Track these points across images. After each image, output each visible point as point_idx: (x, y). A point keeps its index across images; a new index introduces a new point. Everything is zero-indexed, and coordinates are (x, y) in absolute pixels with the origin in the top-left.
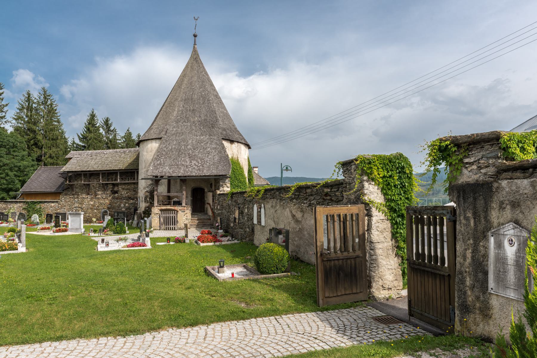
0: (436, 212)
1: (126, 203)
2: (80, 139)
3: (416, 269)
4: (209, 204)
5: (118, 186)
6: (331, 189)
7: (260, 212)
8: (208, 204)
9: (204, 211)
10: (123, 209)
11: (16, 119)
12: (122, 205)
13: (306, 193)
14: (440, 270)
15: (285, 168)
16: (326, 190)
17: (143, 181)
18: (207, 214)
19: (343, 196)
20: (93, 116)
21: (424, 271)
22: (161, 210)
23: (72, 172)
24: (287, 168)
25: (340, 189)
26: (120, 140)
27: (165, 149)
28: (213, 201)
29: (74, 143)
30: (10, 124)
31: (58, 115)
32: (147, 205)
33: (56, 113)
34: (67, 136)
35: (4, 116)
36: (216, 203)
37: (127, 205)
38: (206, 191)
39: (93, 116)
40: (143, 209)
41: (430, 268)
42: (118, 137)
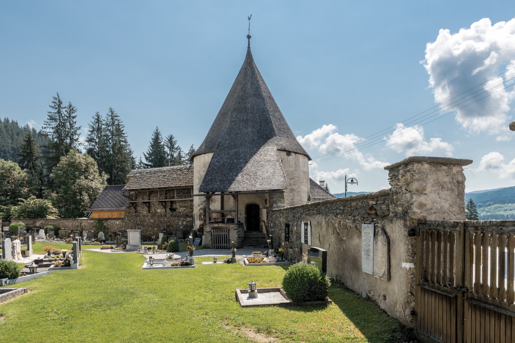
0: (504, 228)
1: (184, 221)
2: (147, 159)
3: (475, 306)
4: (264, 222)
5: (175, 204)
6: (377, 201)
7: (307, 229)
8: (263, 221)
9: (259, 229)
10: (181, 227)
11: (88, 141)
12: (180, 223)
13: (351, 207)
14: (506, 309)
15: (350, 181)
16: (371, 202)
17: (198, 197)
18: (262, 232)
19: (389, 210)
20: (157, 136)
21: (485, 309)
22: (214, 228)
23: (133, 190)
24: (352, 181)
25: (386, 202)
26: (184, 158)
27: (217, 164)
28: (267, 219)
29: (141, 162)
30: (83, 147)
31: (125, 135)
32: (202, 222)
33: (124, 134)
34: (134, 155)
35: (78, 139)
36: (269, 220)
37: (184, 223)
38: (261, 207)
39: (157, 136)
40: (198, 227)
41: (493, 305)
42: (183, 155)
